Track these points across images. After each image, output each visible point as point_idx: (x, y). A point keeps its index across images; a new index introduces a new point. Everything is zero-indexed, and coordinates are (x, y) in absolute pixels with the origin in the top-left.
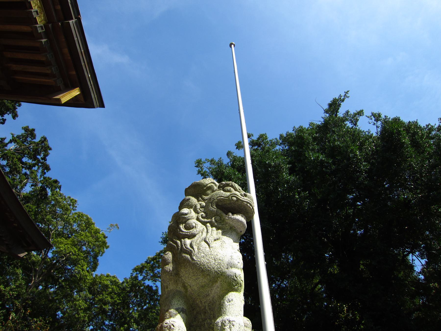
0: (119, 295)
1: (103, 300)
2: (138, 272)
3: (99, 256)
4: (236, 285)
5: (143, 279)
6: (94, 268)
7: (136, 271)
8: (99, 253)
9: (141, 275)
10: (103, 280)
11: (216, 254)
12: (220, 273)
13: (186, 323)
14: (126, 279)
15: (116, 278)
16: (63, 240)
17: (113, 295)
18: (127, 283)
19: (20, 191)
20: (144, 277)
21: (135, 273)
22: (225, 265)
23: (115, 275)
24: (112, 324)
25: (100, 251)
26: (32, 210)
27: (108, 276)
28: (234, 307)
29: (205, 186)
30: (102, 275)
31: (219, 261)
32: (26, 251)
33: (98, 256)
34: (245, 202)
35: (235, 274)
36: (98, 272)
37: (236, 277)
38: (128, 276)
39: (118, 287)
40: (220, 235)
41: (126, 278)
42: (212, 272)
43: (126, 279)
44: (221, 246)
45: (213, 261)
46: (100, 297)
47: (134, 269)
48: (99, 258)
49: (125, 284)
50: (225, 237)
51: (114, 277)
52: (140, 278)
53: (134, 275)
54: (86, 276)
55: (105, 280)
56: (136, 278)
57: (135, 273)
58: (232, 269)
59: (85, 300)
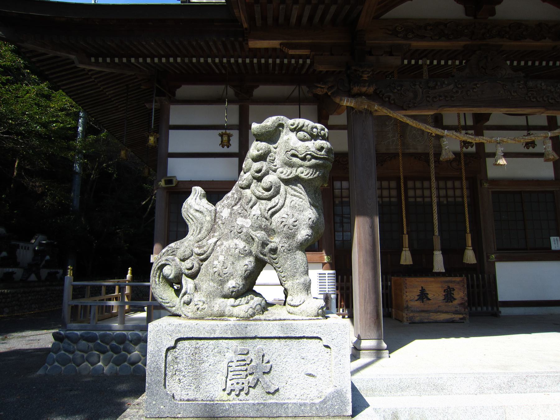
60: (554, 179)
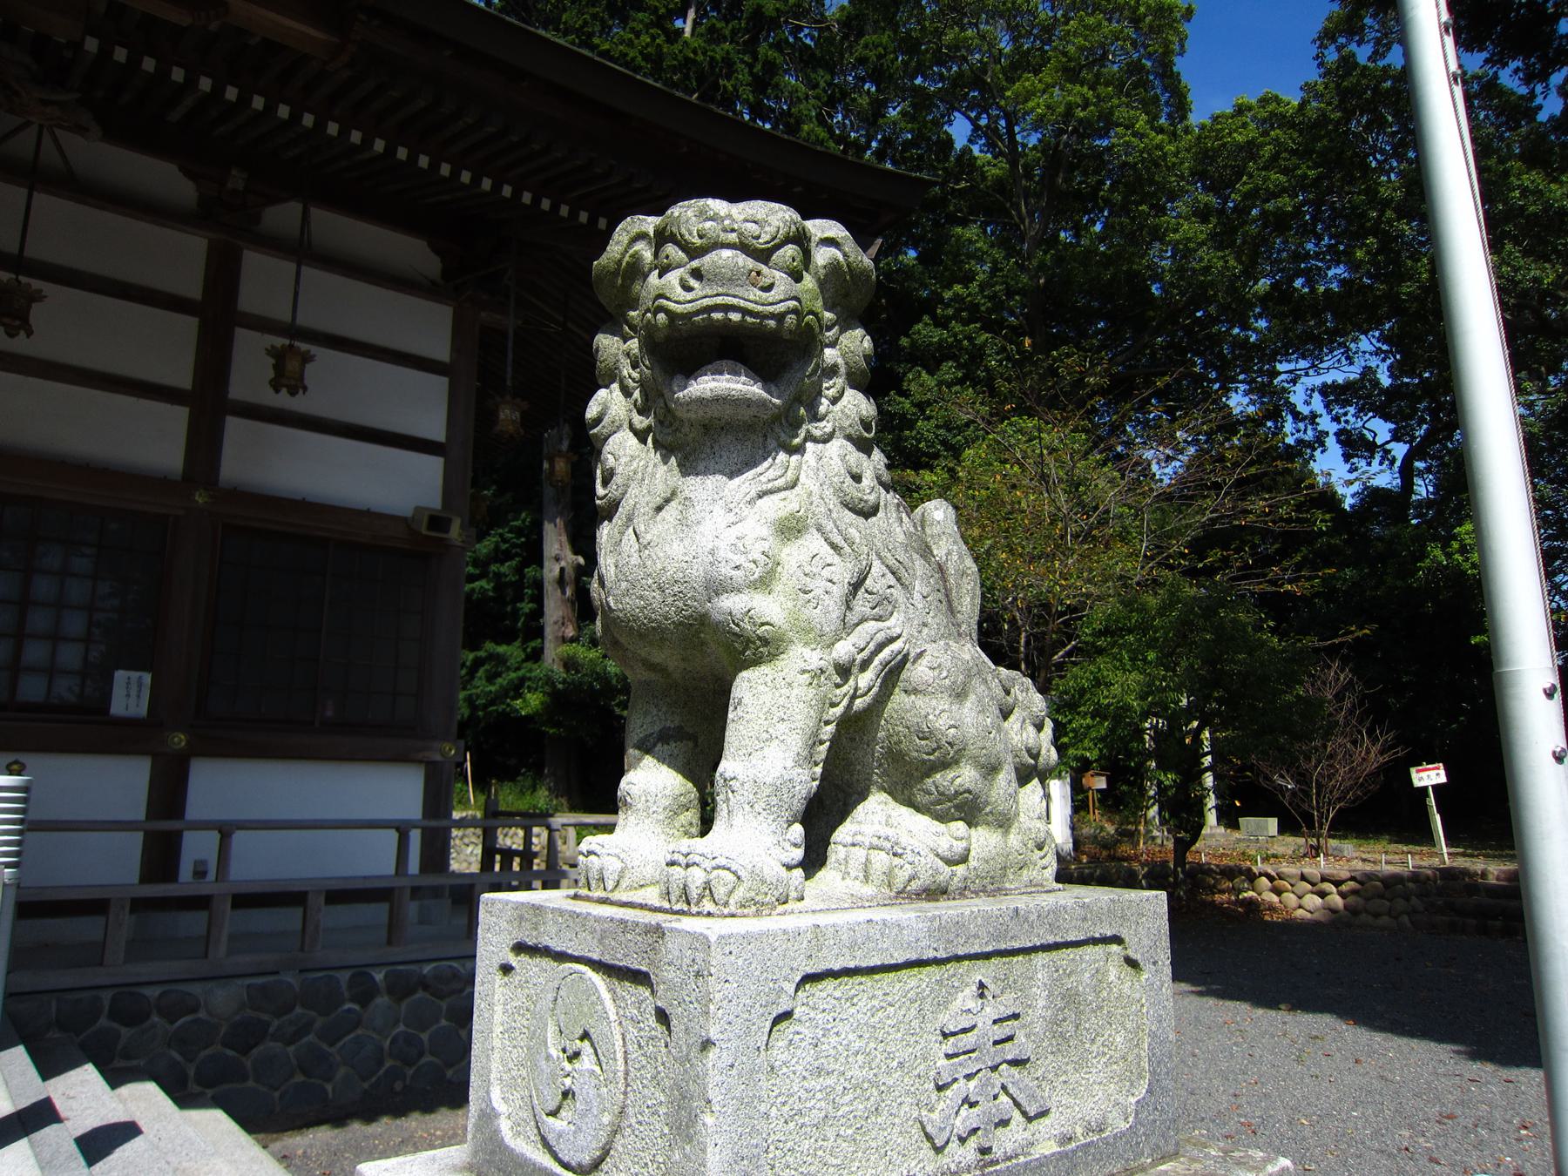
0: (1303, 153)
1: (1257, 192)
2: (1342, 40)
3: (1176, 59)
4: (746, 648)
5: (1375, 52)
6: (1181, 108)
7: (1334, 40)
8: (1168, 52)
9: (1359, 44)
10: (1230, 134)
11: (659, 566)
12: (696, 620)
13: (691, 771)
14: (1308, 88)
15: (1277, 99)
16: (1028, 81)
17: (1284, 159)
18: (1319, 96)
19: (822, 15)
20: (1378, 42)
21: (1333, 46)
22: (700, 590)
23: (1263, 91)
24: (1330, 246)
25: (1166, 44)
26: (885, 49)
27: (1240, 110)
28: (741, 727)
29: (616, 273)
30: (1215, 119)
31: (676, 589)
32: (876, 237)
33: (1172, 63)
34: (698, 313)
35: (730, 614)
36: (1197, 118)
37: (737, 625)
38: (1313, 75)
39: (1293, 125)
40: (675, 479)
41: (1306, 84)
42: (666, 628)
43: (1308, 88)
44: (683, 523)
45: (657, 594)
46: (1244, 186)
47: (1319, 38)
48: (1180, 65)
49: (1314, 104)
50: (691, 480)
51: (1264, 101)
52: (1363, 54)
53: (1332, 56)
54: (1159, 147)
55: (1235, 131)
56: (1348, 62)
57: (1333, 46)
58: (722, 598)
59: (1203, 214)
60: (179, 478)
